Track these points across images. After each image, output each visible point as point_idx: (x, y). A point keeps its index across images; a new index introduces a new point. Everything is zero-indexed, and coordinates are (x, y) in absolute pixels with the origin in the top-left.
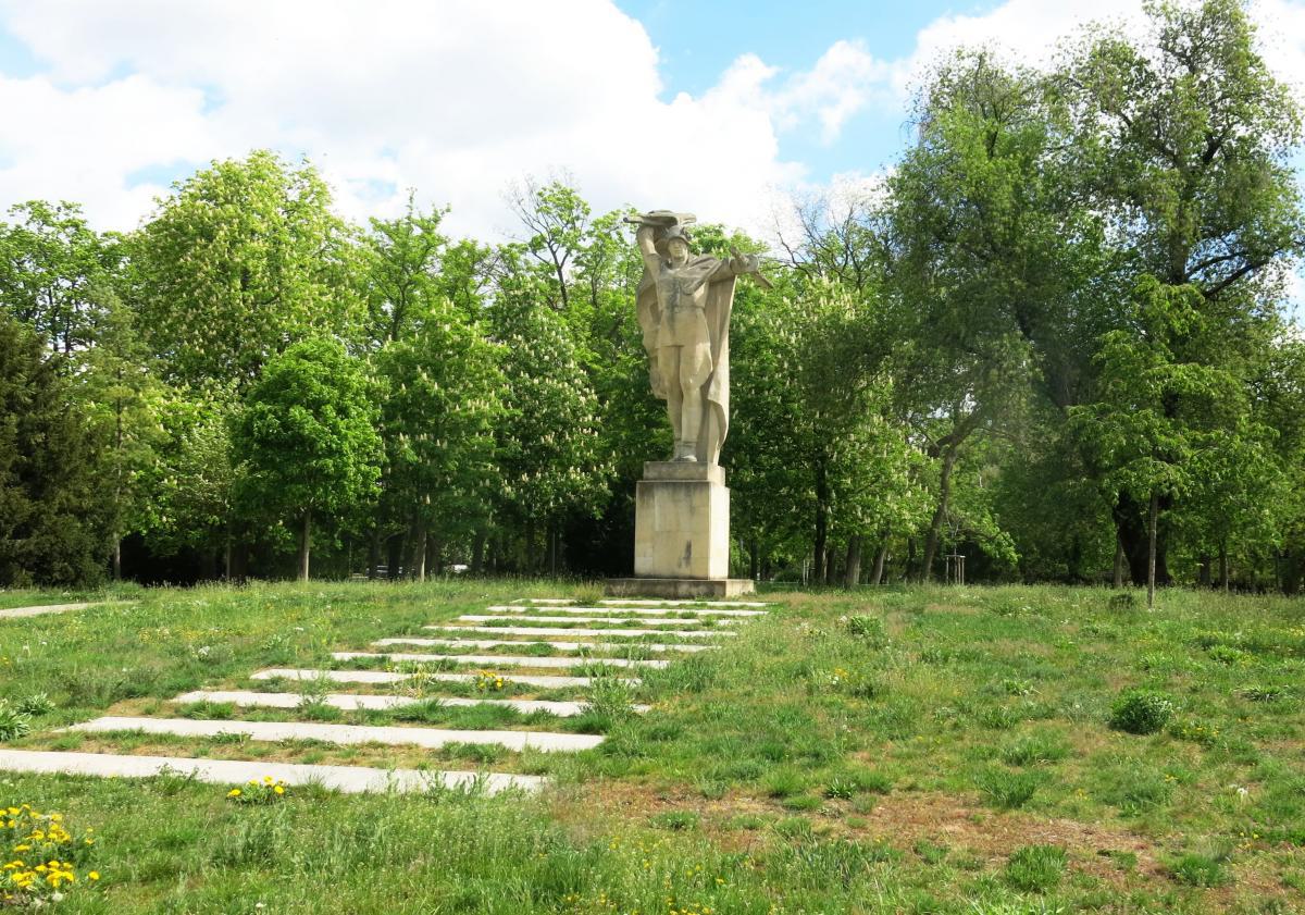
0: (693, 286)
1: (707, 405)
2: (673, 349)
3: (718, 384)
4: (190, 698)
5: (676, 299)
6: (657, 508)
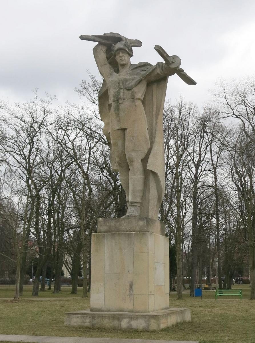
2: (119, 132)
5: (120, 93)
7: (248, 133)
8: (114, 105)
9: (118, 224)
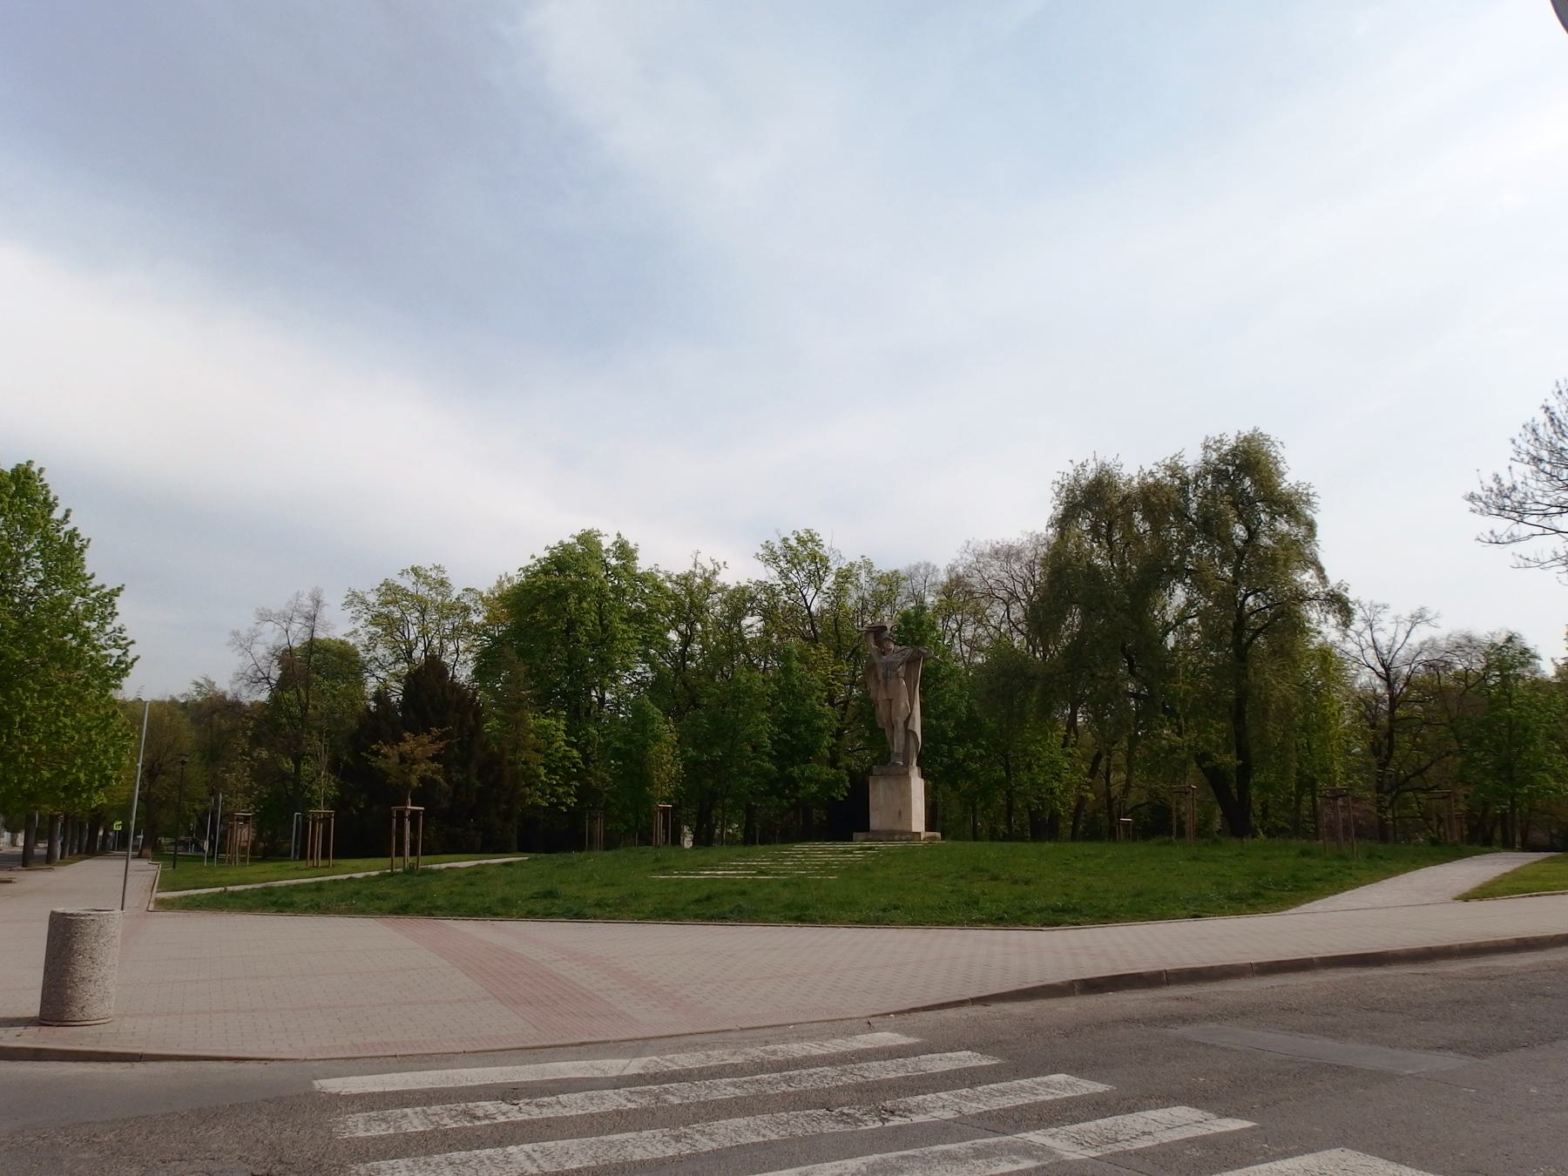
1: (909, 733)
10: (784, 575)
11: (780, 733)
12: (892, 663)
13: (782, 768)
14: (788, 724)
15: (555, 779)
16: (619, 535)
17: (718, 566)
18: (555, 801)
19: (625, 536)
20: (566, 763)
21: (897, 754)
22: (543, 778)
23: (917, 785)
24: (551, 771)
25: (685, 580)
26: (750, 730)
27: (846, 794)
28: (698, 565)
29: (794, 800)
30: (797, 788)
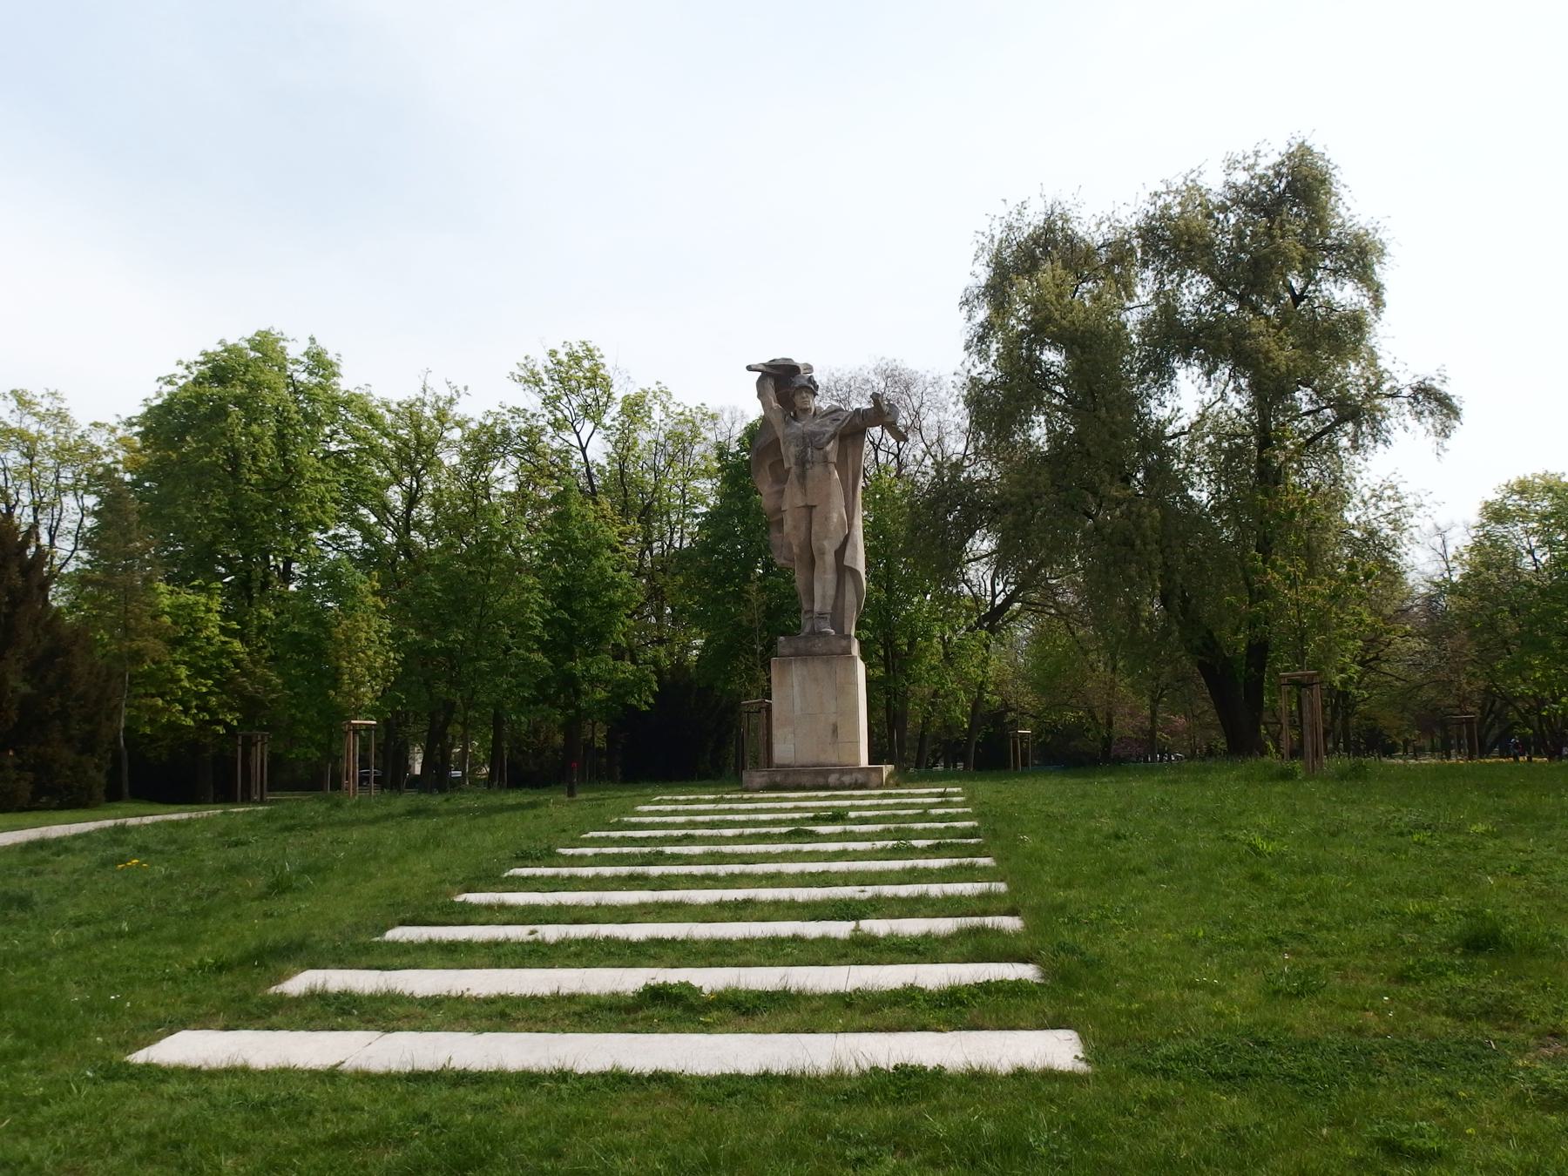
0: (824, 440)
1: (843, 571)
2: (804, 510)
3: (855, 546)
4: (299, 983)
5: (806, 454)
6: (796, 689)
7: (958, 467)
8: (794, 470)
9: (809, 644)
10: (551, 402)
11: (554, 610)
12: (813, 434)
13: (557, 664)
14: (565, 597)
15: (205, 685)
16: (312, 340)
17: (457, 391)
18: (208, 718)
19: (323, 343)
20: (224, 661)
21: (821, 615)
22: (186, 684)
23: (861, 667)
24: (198, 672)
25: (410, 412)
26: (509, 601)
27: (651, 700)
28: (428, 390)
29: (573, 711)
30: (578, 693)
